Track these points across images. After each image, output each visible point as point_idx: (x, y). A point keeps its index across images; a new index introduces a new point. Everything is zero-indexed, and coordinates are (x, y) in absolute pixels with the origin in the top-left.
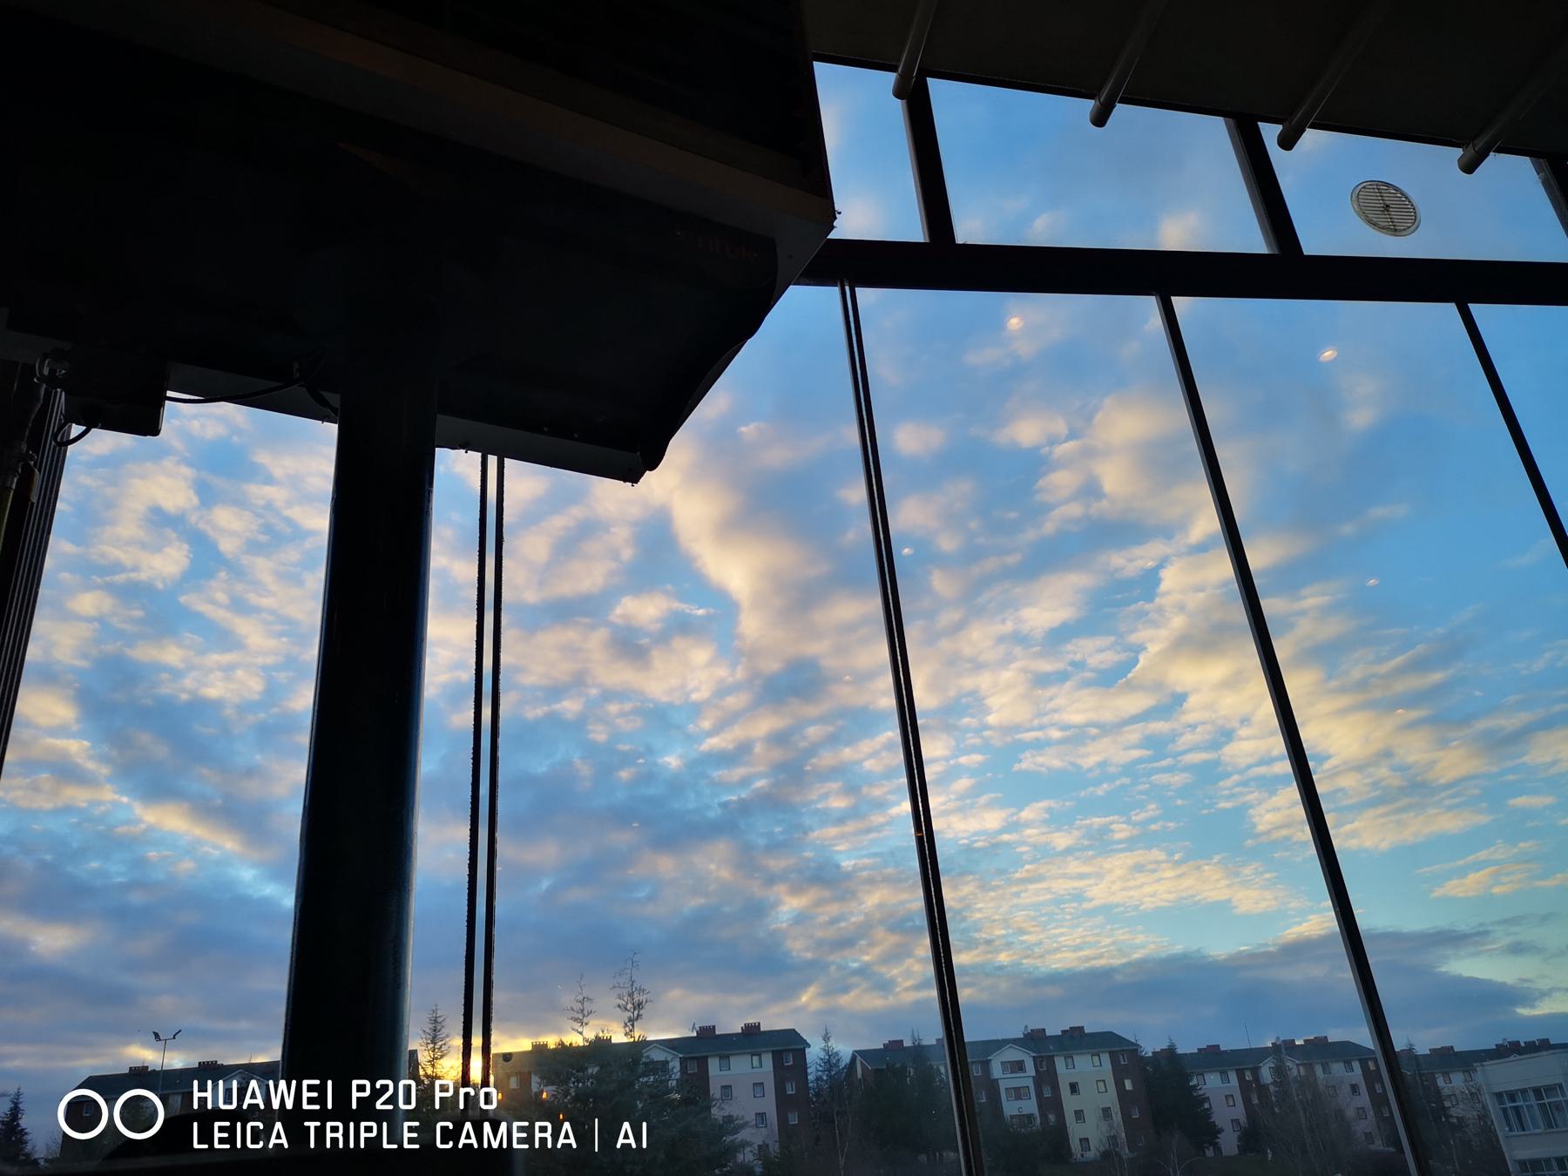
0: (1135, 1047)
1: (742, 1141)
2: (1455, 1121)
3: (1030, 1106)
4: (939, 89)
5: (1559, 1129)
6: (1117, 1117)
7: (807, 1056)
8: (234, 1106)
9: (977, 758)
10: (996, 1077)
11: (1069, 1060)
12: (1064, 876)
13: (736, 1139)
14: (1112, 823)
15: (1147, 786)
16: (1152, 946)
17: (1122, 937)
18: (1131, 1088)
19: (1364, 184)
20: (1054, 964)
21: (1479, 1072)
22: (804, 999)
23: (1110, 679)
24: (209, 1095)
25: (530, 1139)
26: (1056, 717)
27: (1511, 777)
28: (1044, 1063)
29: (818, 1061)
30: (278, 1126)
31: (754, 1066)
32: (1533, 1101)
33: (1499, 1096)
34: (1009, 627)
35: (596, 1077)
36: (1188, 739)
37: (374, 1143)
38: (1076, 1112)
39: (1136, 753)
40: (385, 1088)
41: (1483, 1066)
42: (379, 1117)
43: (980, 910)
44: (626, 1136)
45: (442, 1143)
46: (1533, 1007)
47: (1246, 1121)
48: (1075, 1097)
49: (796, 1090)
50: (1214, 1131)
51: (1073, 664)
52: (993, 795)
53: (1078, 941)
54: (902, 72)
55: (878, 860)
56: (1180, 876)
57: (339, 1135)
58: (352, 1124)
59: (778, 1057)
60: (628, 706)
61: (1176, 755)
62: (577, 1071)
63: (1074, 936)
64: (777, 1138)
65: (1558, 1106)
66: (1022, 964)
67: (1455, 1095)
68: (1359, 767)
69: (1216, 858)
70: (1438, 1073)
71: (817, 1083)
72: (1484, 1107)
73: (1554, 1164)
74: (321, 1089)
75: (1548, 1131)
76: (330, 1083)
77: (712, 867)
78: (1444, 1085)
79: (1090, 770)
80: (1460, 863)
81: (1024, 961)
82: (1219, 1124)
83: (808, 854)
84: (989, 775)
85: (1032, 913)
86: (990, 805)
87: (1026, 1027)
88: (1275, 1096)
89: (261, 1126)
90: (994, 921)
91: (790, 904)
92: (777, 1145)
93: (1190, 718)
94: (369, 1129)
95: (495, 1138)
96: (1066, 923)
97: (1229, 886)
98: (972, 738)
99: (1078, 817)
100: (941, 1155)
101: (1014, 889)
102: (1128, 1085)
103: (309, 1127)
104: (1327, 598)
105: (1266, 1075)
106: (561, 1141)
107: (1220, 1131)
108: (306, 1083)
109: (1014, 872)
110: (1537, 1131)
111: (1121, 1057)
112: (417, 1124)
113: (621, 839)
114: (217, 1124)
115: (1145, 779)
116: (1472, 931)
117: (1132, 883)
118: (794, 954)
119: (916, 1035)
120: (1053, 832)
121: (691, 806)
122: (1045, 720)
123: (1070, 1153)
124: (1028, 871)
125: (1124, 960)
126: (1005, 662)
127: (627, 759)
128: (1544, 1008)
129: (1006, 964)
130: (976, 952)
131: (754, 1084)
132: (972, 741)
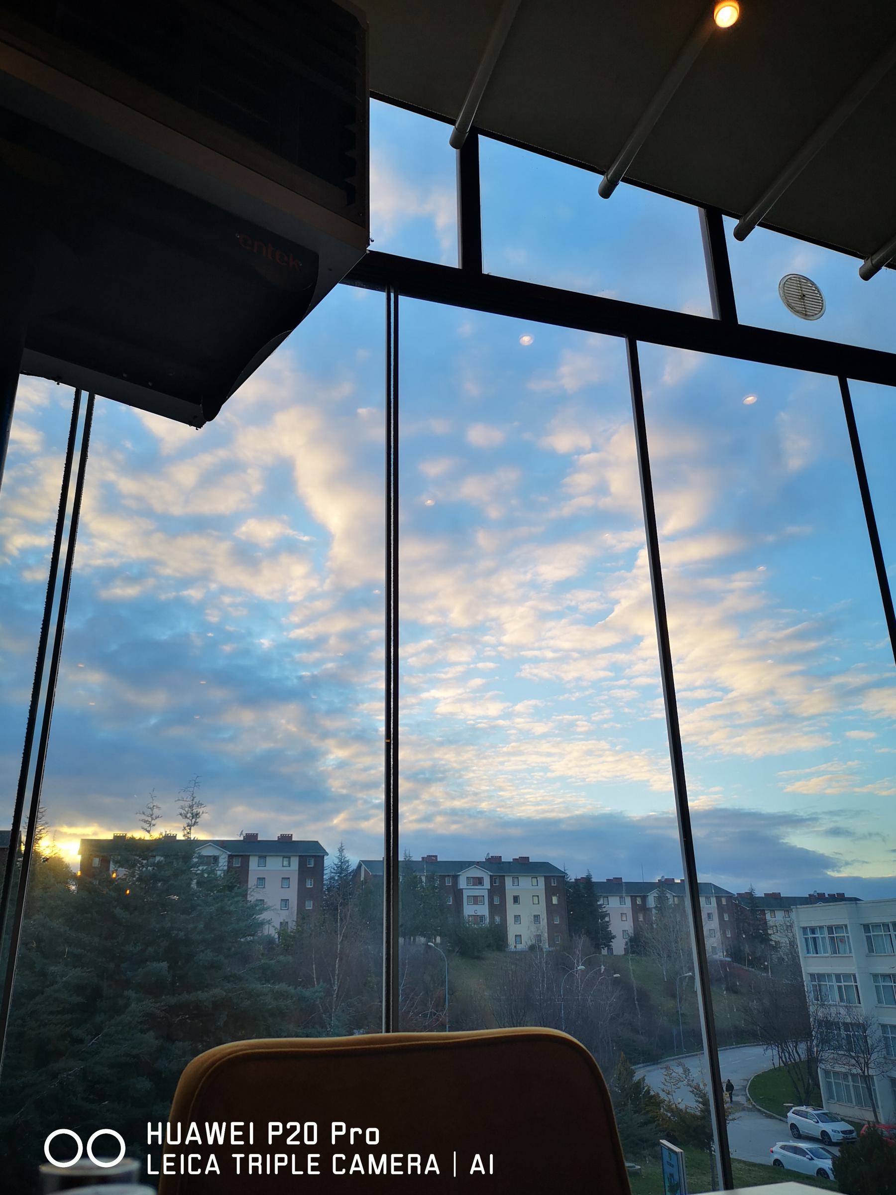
0: (563, 875)
1: (264, 919)
2: (774, 943)
4: (487, 146)
5: (840, 955)
7: (325, 861)
8: (178, 1142)
9: (491, 665)
10: (461, 888)
11: (516, 880)
12: (537, 753)
13: (260, 918)
15: (606, 697)
16: (590, 807)
19: (789, 277)
20: (519, 813)
22: (335, 821)
24: (159, 1133)
25: (404, 1168)
26: (552, 643)
27: (850, 717)
28: (497, 881)
30: (212, 1157)
31: (284, 865)
32: (826, 935)
34: (529, 577)
37: (285, 1170)
39: (602, 674)
40: (294, 1128)
41: (797, 908)
42: (289, 1150)
43: (474, 771)
44: (477, 1165)
46: (838, 871)
47: (633, 932)
48: (516, 906)
49: (314, 885)
50: (609, 937)
51: (570, 608)
52: (496, 692)
53: (539, 799)
54: (459, 125)
55: (407, 728)
56: (617, 761)
57: (259, 1164)
58: (268, 1156)
60: (239, 599)
61: (630, 678)
63: (537, 795)
65: (842, 940)
66: (496, 811)
69: (645, 751)
72: (793, 936)
73: (834, 977)
74: (245, 1129)
76: (251, 1124)
77: (283, 721)
79: (569, 682)
81: (498, 809)
85: (510, 777)
86: (493, 699)
87: (488, 854)
88: (655, 917)
89: (199, 1157)
90: (483, 779)
96: (533, 786)
97: (649, 771)
98: (490, 651)
100: (414, 939)
101: (501, 759)
102: (555, 900)
103: (236, 1158)
104: (749, 583)
105: (651, 901)
106: (428, 1169)
107: (614, 937)
108: (233, 1124)
109: (503, 747)
111: (552, 880)
112: (318, 1156)
113: (218, 694)
115: (606, 692)
116: (808, 817)
118: (333, 790)
119: (407, 852)
120: (534, 722)
121: (274, 676)
122: (544, 643)
123: (507, 945)
125: (568, 815)
126: (523, 599)
127: (229, 637)
128: (845, 873)
130: (466, 800)
132: (489, 653)
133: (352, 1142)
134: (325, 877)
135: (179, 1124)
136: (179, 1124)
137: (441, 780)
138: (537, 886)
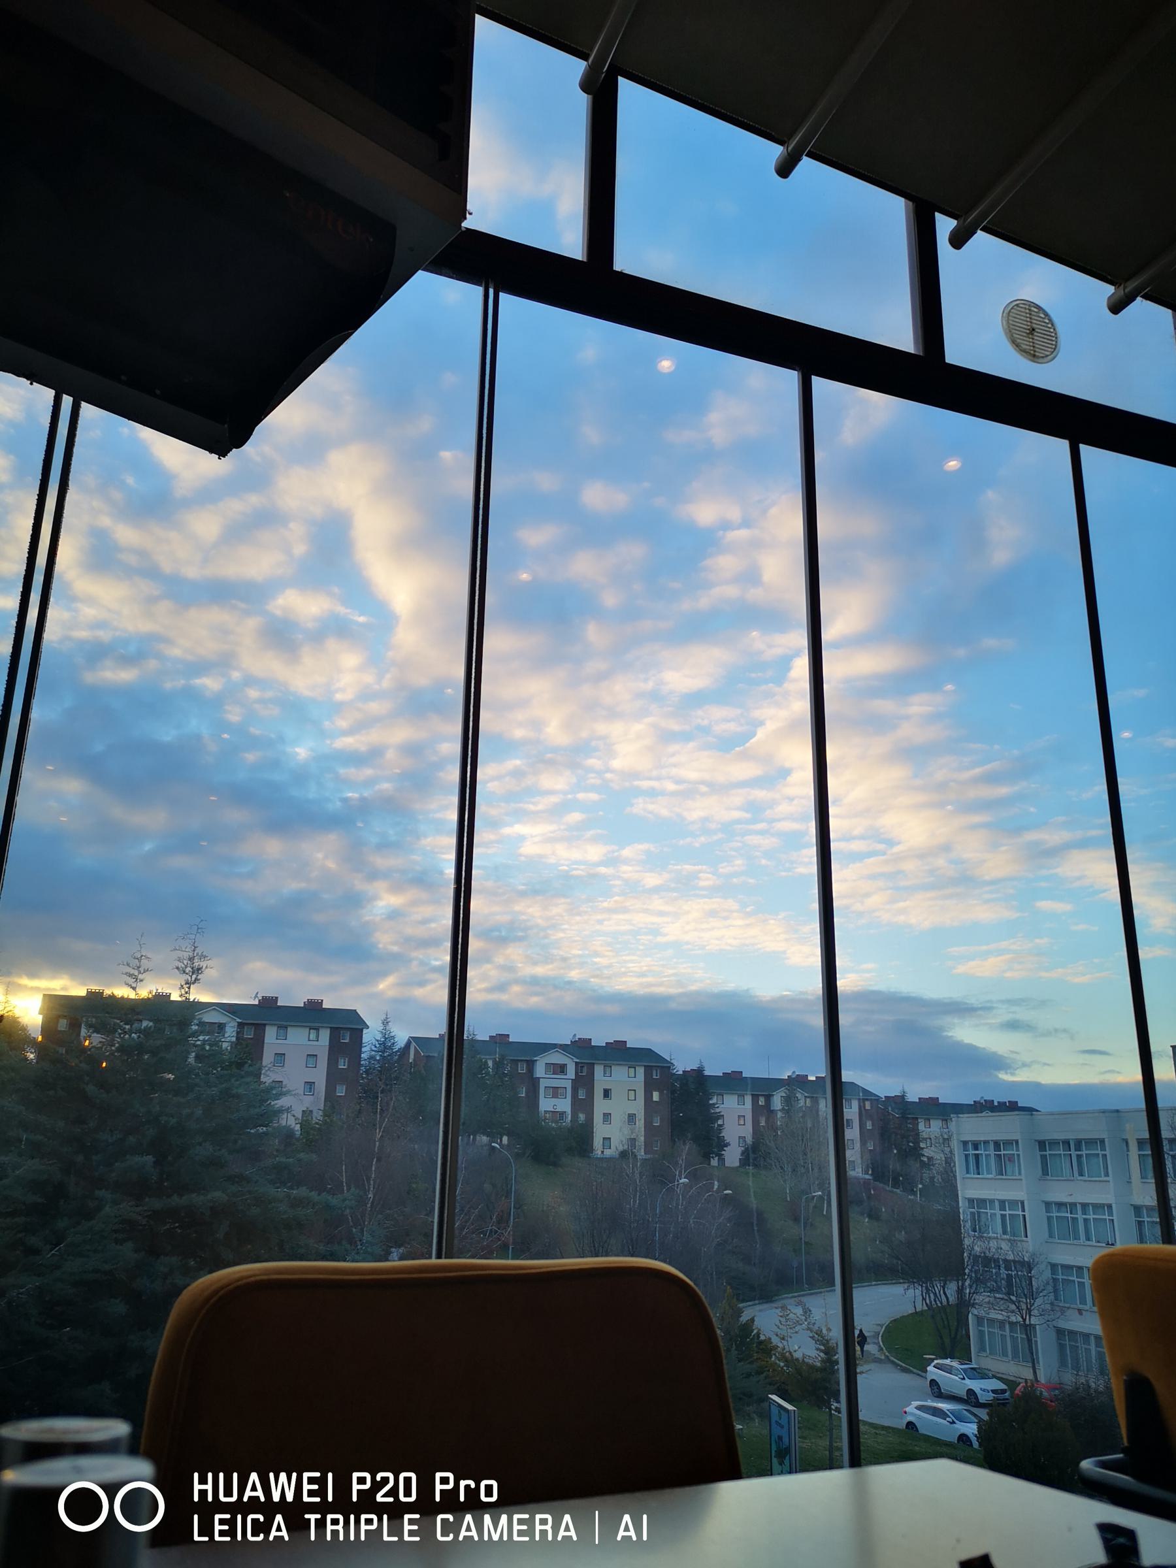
0: (669, 1065)
2: (925, 1159)
3: (564, 1105)
4: (629, 92)
6: (640, 1123)
8: (234, 1498)
9: (593, 796)
12: (646, 911)
13: (276, 1104)
14: (701, 872)
17: (683, 971)
18: (658, 1100)
21: (954, 1123)
23: (729, 745)
24: (209, 1487)
25: (530, 1532)
26: (674, 771)
28: (585, 1069)
29: (374, 1041)
30: (279, 1518)
31: (311, 1038)
32: (992, 1152)
33: (965, 1143)
34: (650, 685)
35: (146, 1032)
36: (783, 808)
38: (605, 1114)
39: (736, 814)
40: (385, 1481)
42: (380, 1509)
43: (563, 931)
45: (442, 1536)
46: (1013, 1074)
48: (607, 1101)
49: (348, 1065)
50: (723, 1145)
54: (593, 61)
56: (748, 925)
59: (335, 1033)
62: (125, 1024)
63: (642, 964)
64: (322, 1107)
65: (1011, 1158)
67: (930, 1138)
68: (922, 855)
69: (782, 915)
70: (921, 1118)
71: (370, 1062)
72: (951, 1152)
74: (322, 1482)
75: (998, 1177)
76: (330, 1475)
78: (924, 1129)
80: (984, 948)
81: (592, 980)
82: (728, 1139)
83: (415, 857)
84: (601, 813)
86: (595, 840)
87: (575, 1035)
89: (262, 1518)
91: (386, 900)
92: (321, 1113)
93: (789, 791)
94: (369, 1522)
95: (496, 1531)
97: (786, 940)
99: (672, 862)
101: (599, 917)
103: (310, 1519)
104: (930, 709)
105: (777, 1103)
106: (562, 1533)
107: (727, 1145)
109: (602, 902)
110: (990, 1176)
113: (235, 816)
114: (217, 1517)
115: (738, 838)
117: (704, 926)
118: (381, 946)
123: (592, 1150)
124: (616, 901)
125: (680, 990)
128: (1022, 1076)
129: (575, 980)
130: (550, 966)
131: (308, 1055)
132: (593, 781)
133: (462, 1499)
134: (362, 1055)
135: (235, 1475)
136: (235, 1475)
137: (521, 939)
138: (635, 1077)
